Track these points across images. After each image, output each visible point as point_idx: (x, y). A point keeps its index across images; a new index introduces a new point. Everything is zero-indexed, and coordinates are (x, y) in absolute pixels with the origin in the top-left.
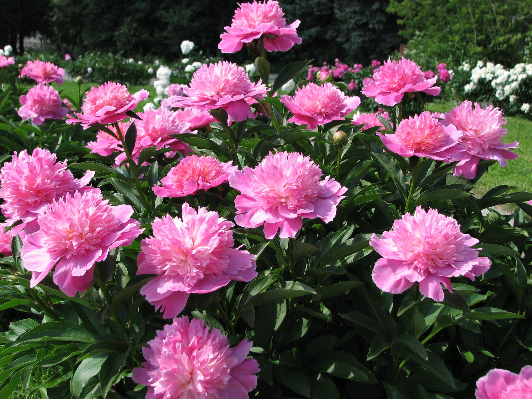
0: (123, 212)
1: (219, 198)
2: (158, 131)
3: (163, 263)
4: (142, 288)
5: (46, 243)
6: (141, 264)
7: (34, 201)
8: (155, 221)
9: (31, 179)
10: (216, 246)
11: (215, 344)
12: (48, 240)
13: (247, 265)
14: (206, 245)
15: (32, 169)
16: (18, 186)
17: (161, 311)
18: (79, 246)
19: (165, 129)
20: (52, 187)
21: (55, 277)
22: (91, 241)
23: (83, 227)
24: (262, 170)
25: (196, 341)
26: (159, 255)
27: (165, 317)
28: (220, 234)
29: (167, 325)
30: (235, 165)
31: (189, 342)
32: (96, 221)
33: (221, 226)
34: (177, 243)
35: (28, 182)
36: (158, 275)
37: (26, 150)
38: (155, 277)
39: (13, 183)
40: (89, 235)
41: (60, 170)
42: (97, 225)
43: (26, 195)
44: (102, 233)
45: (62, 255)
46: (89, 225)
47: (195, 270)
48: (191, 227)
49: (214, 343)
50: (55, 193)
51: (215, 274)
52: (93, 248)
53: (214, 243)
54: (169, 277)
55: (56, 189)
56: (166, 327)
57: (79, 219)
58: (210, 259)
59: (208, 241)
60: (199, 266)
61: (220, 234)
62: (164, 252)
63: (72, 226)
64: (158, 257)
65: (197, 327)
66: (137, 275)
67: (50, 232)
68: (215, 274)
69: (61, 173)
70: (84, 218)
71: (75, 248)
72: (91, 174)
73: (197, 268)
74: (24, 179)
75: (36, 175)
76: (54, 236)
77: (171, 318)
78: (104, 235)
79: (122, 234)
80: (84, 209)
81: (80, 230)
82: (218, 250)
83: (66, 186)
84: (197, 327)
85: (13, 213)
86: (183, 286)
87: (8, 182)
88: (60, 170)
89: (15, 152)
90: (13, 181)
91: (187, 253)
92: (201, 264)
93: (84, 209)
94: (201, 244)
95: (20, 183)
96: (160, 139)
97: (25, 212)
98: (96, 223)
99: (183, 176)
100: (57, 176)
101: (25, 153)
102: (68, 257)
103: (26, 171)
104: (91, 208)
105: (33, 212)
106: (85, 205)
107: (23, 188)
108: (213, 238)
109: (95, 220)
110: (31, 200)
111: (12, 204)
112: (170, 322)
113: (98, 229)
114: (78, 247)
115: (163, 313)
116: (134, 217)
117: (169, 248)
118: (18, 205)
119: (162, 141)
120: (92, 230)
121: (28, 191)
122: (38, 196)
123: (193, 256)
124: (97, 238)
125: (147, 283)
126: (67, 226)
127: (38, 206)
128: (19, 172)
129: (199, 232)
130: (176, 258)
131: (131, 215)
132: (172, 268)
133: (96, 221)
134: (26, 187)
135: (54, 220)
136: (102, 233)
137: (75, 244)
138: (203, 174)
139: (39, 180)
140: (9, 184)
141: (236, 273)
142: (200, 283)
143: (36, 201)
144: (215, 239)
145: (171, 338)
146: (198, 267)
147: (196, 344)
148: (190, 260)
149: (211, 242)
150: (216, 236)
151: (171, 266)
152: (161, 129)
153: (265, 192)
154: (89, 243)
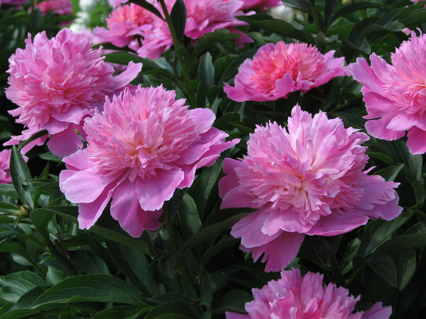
0: (205, 117)
1: (338, 100)
2: (202, 11)
3: (271, 189)
4: (234, 228)
5: (95, 161)
6: (227, 194)
7: (62, 104)
8: (256, 130)
9: (57, 74)
10: (350, 168)
11: (345, 309)
12: (101, 155)
13: (388, 197)
14: (333, 167)
15: (57, 58)
16: (39, 82)
17: (263, 261)
18: (150, 164)
19: (213, 9)
20: (88, 85)
21: (114, 208)
22: (163, 157)
23: (155, 138)
24: (404, 58)
25: (316, 304)
26: (263, 180)
27: (268, 270)
28: (353, 151)
29: (273, 281)
30: (339, 57)
31: (305, 308)
32: (173, 128)
33: (352, 140)
34: (290, 163)
35: (53, 77)
36: (256, 210)
37: (44, 32)
38: (250, 211)
39: (32, 78)
40: (165, 148)
41: (97, 60)
42: (173, 134)
43: (49, 95)
44: (181, 146)
45: (120, 176)
46: (162, 133)
47: (319, 203)
48: (306, 139)
49: (342, 308)
50: (92, 94)
51: (342, 209)
52: (168, 168)
53: (346, 162)
54: (278, 212)
55: (92, 88)
56: (271, 284)
57: (148, 124)
58: (342, 188)
59: (337, 161)
60: (324, 197)
61: (353, 151)
62: (272, 176)
63: (139, 136)
64: (264, 183)
65: (313, 285)
66: (221, 209)
67: (106, 144)
68: (342, 209)
69: (98, 65)
70: (157, 124)
71: (144, 167)
72: (135, 68)
73: (321, 200)
74: (48, 74)
75: (65, 67)
76: (110, 150)
77: (276, 270)
78: (184, 148)
79: (211, 147)
80: (156, 111)
81: (151, 141)
82: (351, 173)
83: (105, 83)
84: (313, 285)
85: (29, 121)
86: (298, 225)
87: (26, 77)
88: (97, 60)
89: (29, 35)
90: (33, 76)
91: (310, 177)
92: (329, 194)
93: (156, 111)
94: (324, 165)
95: (41, 79)
96: (206, 23)
97: (46, 120)
98: (174, 130)
99: (271, 73)
100: (94, 70)
101: (42, 36)
102: (132, 179)
103: (50, 62)
104: (166, 109)
105: (62, 120)
106: (156, 105)
107: (47, 86)
108: (344, 156)
109: (171, 127)
110: (58, 102)
111: (29, 108)
112: (276, 276)
113: (176, 140)
114: (149, 166)
115: (265, 264)
116: (219, 125)
117: (276, 171)
118: (38, 110)
119: (211, 25)
120: (167, 142)
121: (53, 89)
122: (66, 98)
123: (317, 183)
124: (174, 153)
125: (239, 220)
126: (131, 135)
127: (67, 112)
128: (40, 62)
129: (321, 148)
130: (289, 184)
131: (213, 122)
132: (281, 201)
133: (173, 128)
134: (51, 85)
135: (110, 126)
136: (181, 146)
137: (143, 161)
138: (296, 68)
139: (69, 75)
140: (27, 79)
141: (372, 207)
142: (324, 221)
143: (65, 105)
144: (348, 158)
145: (282, 300)
146: (324, 199)
147: (316, 308)
148: (309, 188)
149: (340, 163)
150: (348, 153)
151: (281, 195)
152: (207, 9)
153: (411, 89)
154: (161, 160)
